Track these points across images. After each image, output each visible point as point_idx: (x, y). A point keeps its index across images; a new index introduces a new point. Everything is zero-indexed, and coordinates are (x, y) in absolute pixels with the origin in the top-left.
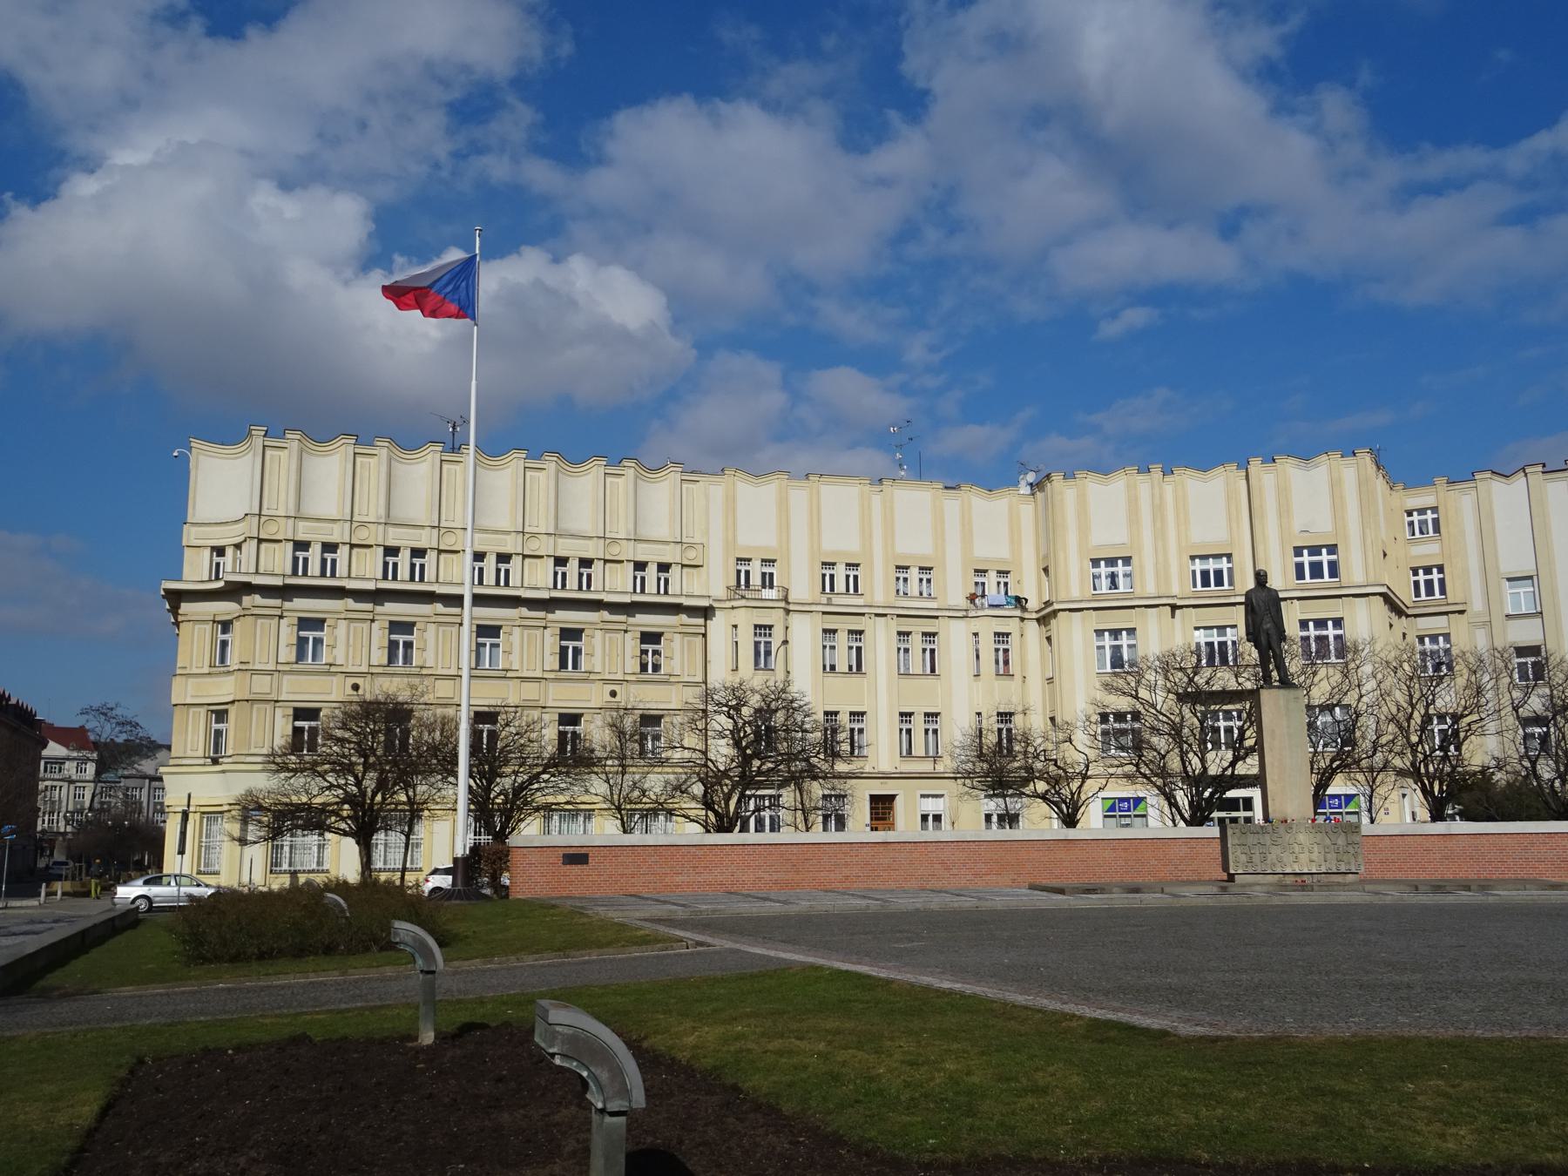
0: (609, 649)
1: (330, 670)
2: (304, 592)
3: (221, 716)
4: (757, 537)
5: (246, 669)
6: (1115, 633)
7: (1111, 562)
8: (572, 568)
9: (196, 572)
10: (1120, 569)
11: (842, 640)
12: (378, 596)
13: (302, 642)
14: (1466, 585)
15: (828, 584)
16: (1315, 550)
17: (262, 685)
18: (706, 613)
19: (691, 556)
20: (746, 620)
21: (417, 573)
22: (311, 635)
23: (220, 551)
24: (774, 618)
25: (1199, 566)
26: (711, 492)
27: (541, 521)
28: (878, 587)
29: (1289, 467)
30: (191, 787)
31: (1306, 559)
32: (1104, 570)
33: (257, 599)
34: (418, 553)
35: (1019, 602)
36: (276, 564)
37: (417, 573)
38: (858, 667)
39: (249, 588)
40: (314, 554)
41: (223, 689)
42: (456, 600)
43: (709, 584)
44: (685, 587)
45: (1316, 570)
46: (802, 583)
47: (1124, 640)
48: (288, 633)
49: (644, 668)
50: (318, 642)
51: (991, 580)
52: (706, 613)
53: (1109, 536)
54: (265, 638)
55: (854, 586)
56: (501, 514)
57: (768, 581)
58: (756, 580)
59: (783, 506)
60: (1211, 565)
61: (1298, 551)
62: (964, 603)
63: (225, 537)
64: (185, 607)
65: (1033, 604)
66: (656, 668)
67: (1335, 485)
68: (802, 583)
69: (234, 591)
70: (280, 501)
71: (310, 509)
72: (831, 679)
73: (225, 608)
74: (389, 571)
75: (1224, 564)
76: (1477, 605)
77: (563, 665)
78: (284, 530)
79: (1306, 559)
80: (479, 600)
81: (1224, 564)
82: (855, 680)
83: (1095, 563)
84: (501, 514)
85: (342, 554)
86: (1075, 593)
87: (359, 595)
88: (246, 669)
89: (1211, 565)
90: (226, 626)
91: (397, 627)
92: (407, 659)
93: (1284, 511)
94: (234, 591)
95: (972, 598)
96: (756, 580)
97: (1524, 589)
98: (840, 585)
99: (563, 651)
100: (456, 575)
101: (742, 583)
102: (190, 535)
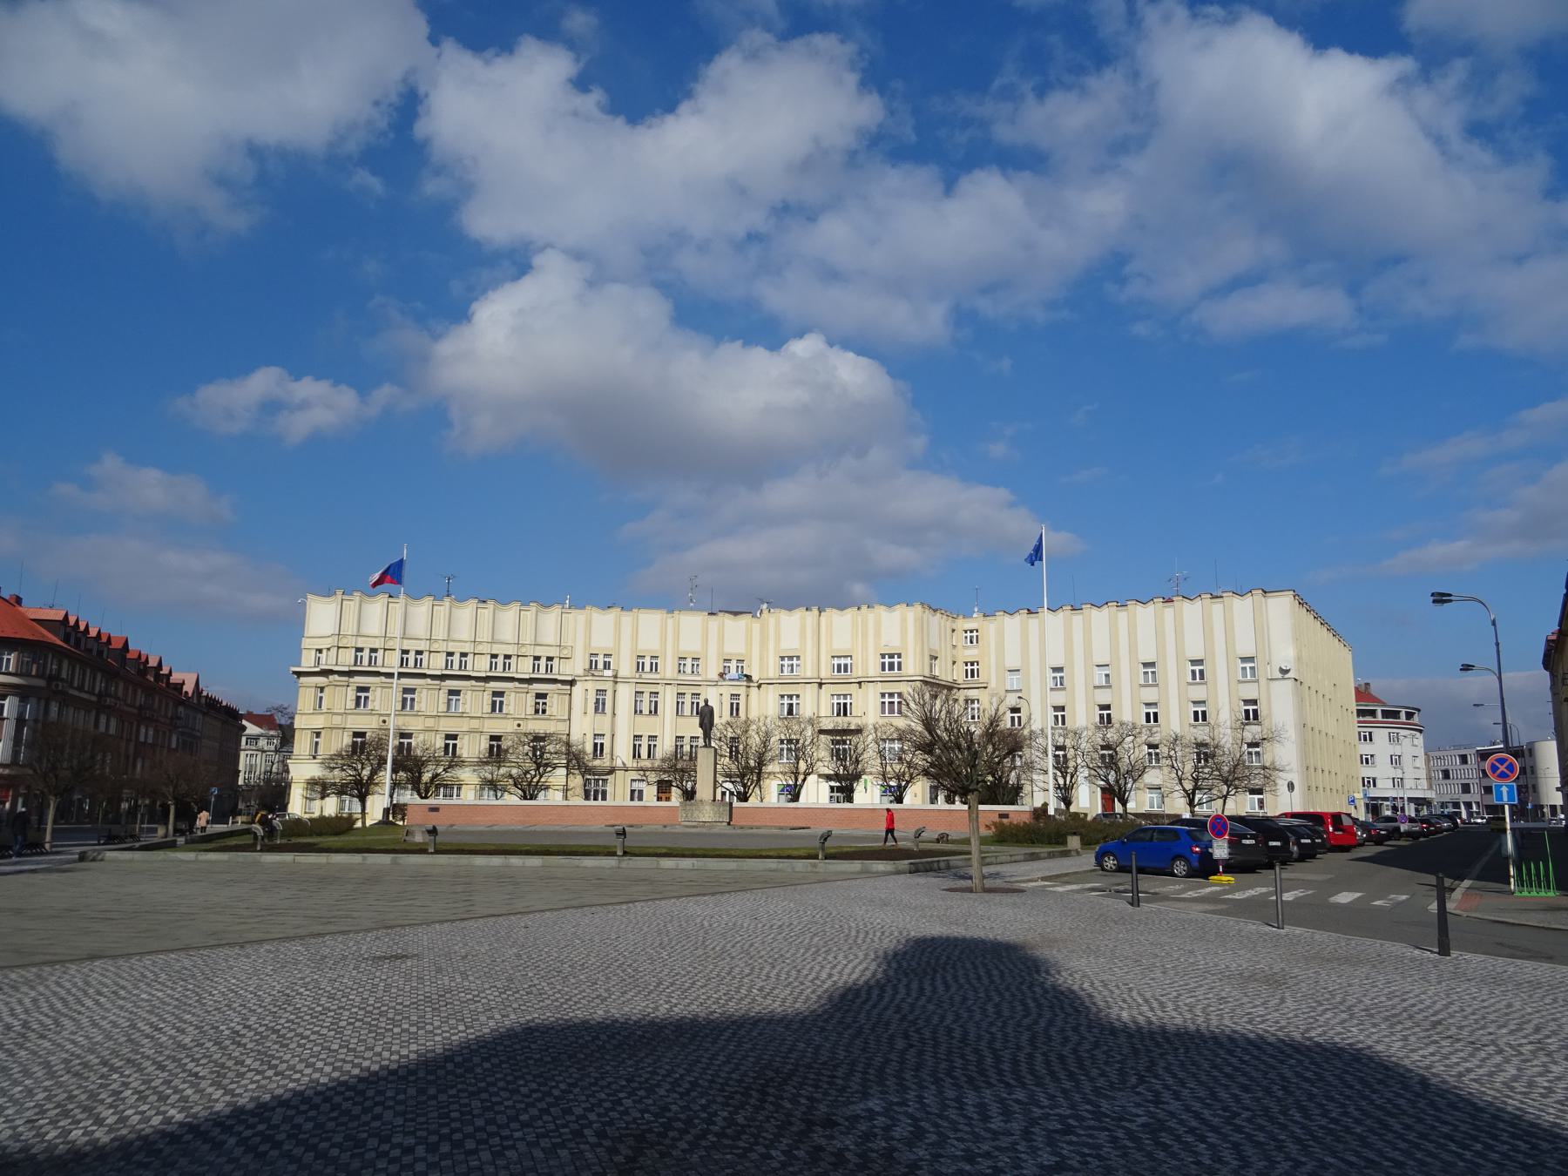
0: (518, 702)
1: (372, 713)
2: (360, 674)
3: (318, 735)
4: (602, 642)
5: (331, 713)
6: (790, 697)
7: (791, 658)
8: (543, 662)
9: (308, 663)
10: (795, 662)
11: (646, 697)
12: (443, 678)
13: (358, 698)
14: (988, 673)
15: (639, 667)
16: (891, 656)
17: (337, 720)
18: (572, 683)
19: (565, 653)
20: (592, 687)
21: (549, 669)
22: (409, 696)
23: (320, 651)
24: (608, 686)
25: (836, 661)
26: (577, 618)
27: (527, 638)
28: (668, 669)
29: (881, 611)
30: (302, 770)
31: (887, 660)
32: (786, 662)
33: (336, 677)
34: (550, 659)
35: (749, 678)
36: (346, 660)
37: (463, 665)
38: (654, 711)
39: (332, 672)
40: (456, 658)
41: (319, 722)
42: (390, 675)
43: (574, 667)
44: (563, 670)
45: (891, 667)
46: (626, 668)
47: (794, 701)
48: (352, 694)
49: (537, 711)
50: (366, 698)
51: (733, 665)
52: (572, 683)
53: (790, 644)
54: (341, 696)
55: (654, 668)
56: (464, 631)
57: (607, 666)
58: (600, 666)
59: (618, 626)
60: (843, 661)
61: (883, 656)
62: (716, 677)
63: (323, 644)
64: (303, 679)
65: (755, 678)
66: (544, 712)
67: (904, 620)
68: (626, 668)
69: (326, 673)
70: (349, 627)
71: (454, 636)
72: (638, 718)
73: (321, 680)
74: (535, 668)
75: (848, 661)
76: (993, 685)
77: (493, 710)
78: (351, 642)
79: (887, 660)
80: (401, 675)
81: (848, 661)
82: (652, 718)
83: (782, 658)
84: (464, 631)
85: (425, 656)
86: (771, 675)
87: (433, 677)
88: (331, 713)
89: (843, 661)
90: (322, 689)
91: (497, 694)
92: (412, 707)
93: (878, 634)
94: (326, 673)
95: (721, 675)
96: (600, 666)
97: (1015, 677)
98: (647, 668)
99: (494, 703)
100: (392, 663)
101: (592, 665)
102: (306, 643)
